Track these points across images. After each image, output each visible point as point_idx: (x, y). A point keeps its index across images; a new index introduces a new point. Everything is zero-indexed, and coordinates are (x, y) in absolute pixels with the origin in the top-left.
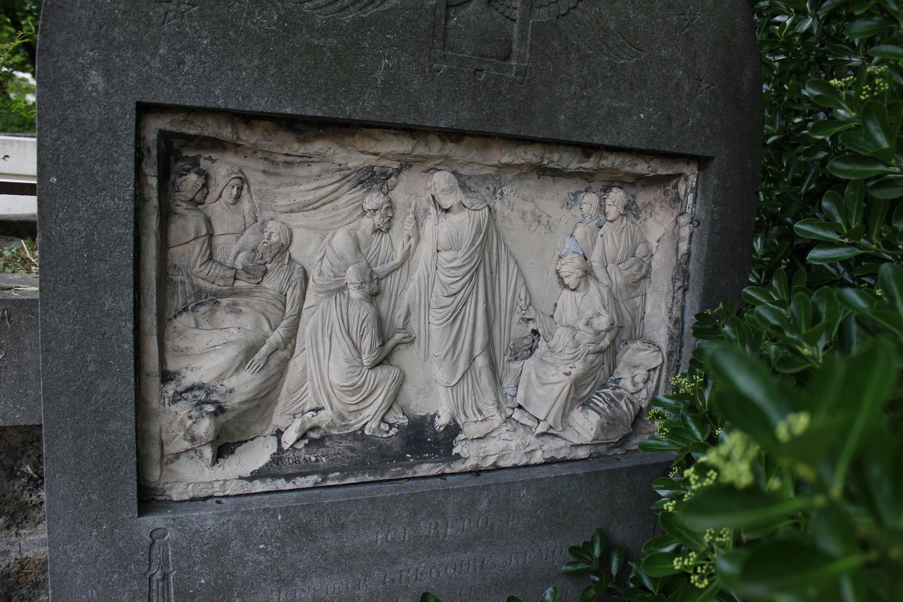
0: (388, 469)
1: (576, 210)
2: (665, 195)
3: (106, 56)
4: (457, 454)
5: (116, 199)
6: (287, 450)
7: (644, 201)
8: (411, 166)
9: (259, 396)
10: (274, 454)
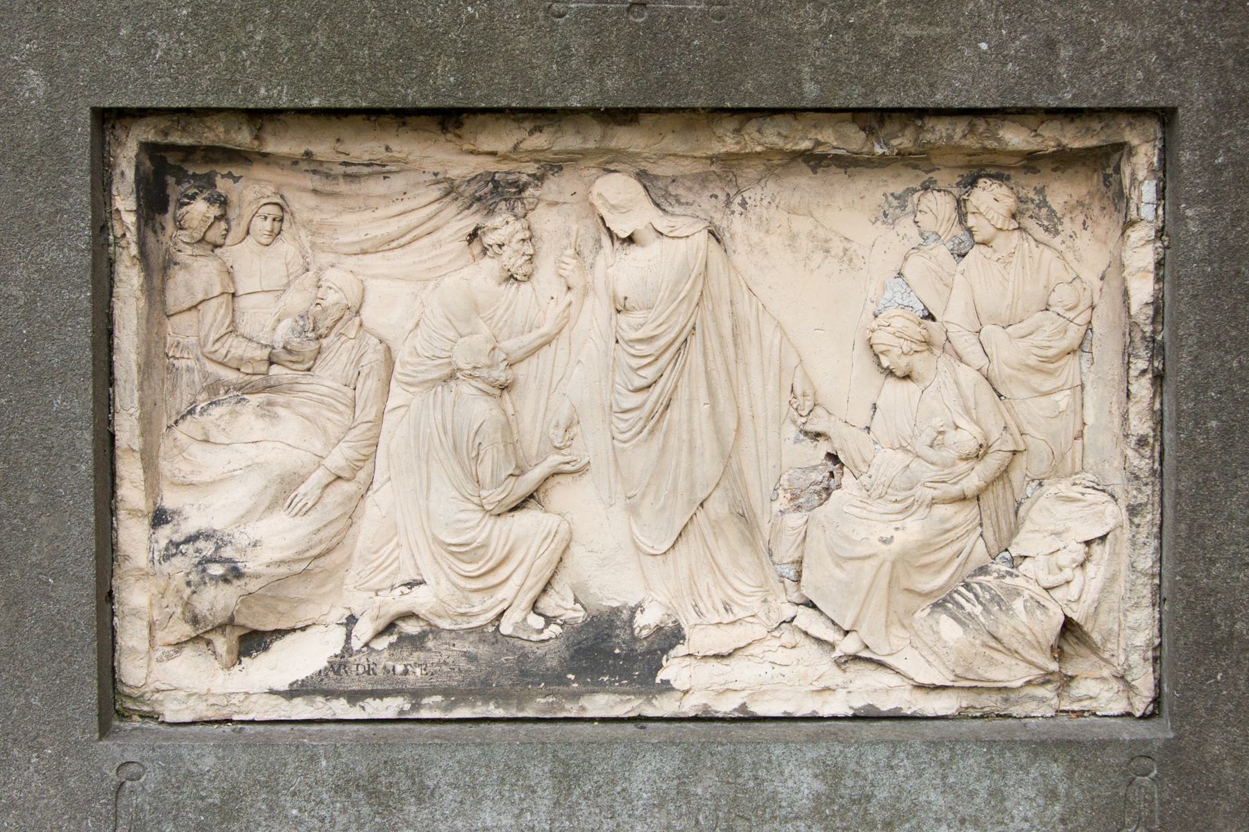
0: (531, 698)
2: (1105, 185)
3: (46, 47)
4: (666, 682)
5: (66, 250)
6: (359, 651)
7: (1066, 198)
8: (561, 168)
9: (308, 554)
10: (336, 656)
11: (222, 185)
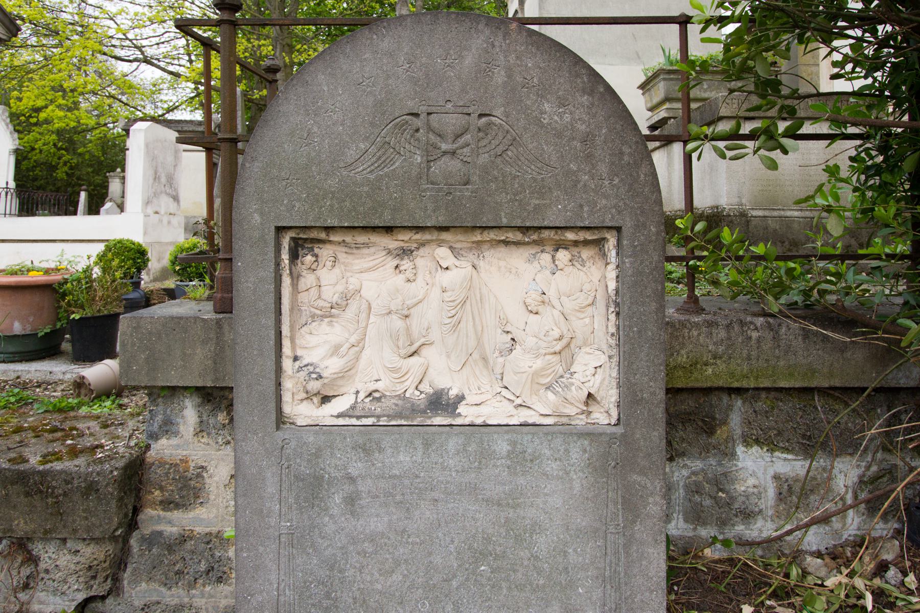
0: (416, 418)
1: (536, 264)
4: (459, 413)
11: (316, 250)
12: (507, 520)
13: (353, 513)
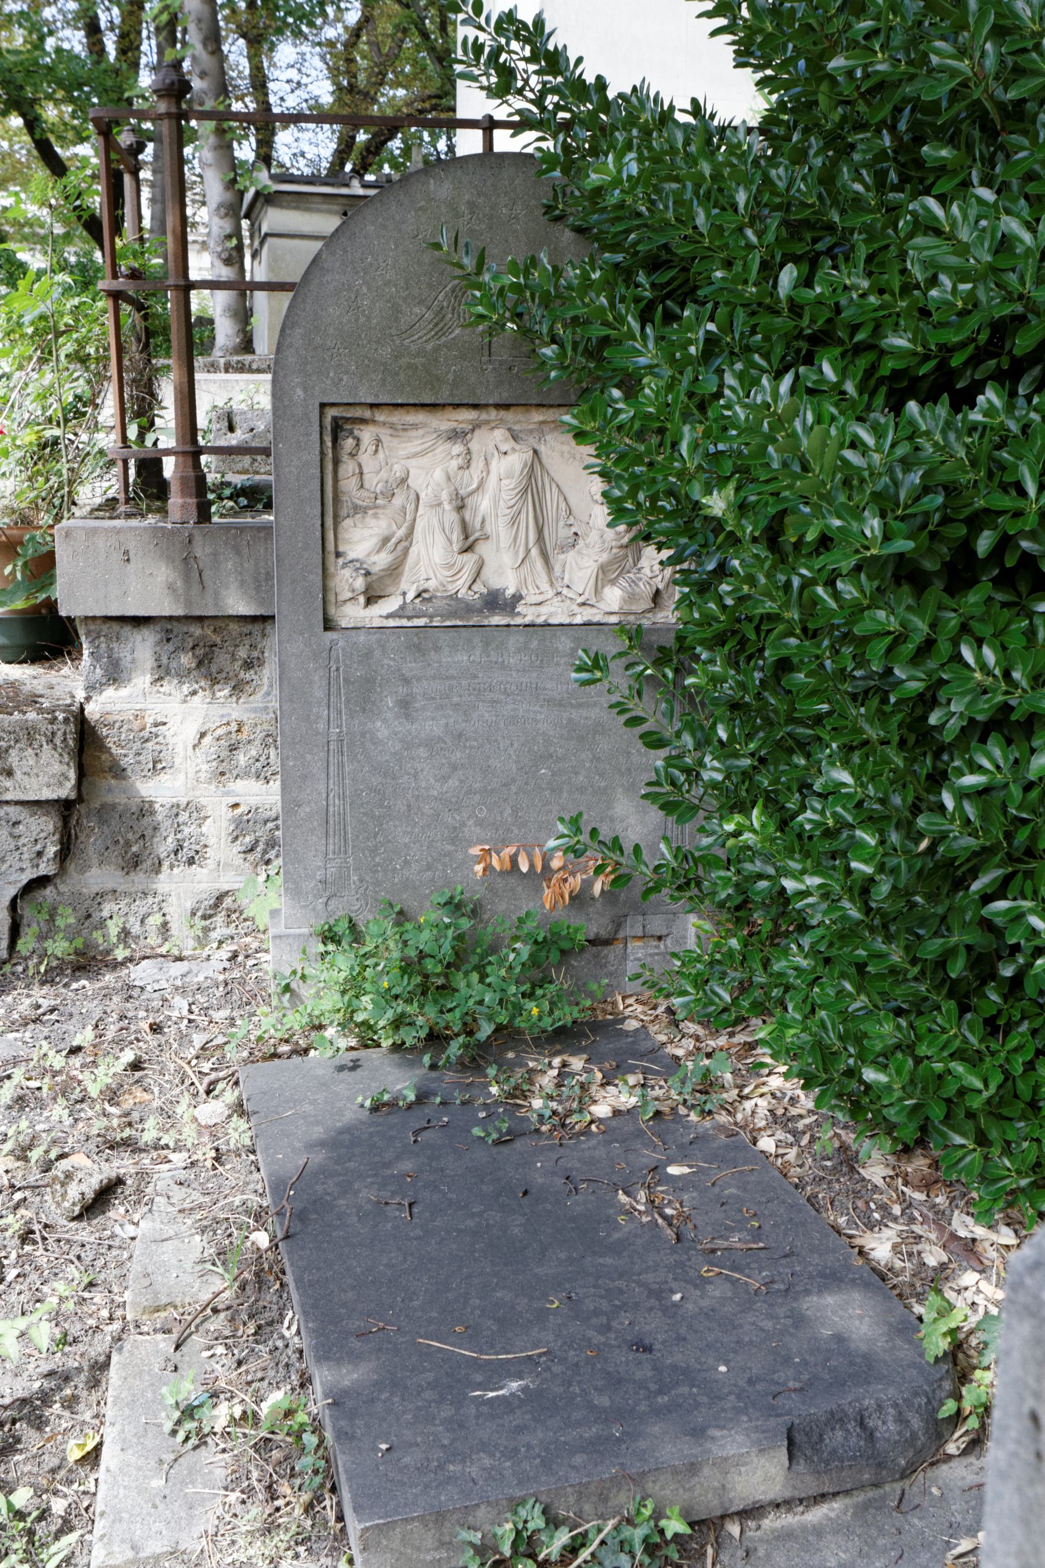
11: (356, 432)
12: (570, 720)
13: (407, 716)
